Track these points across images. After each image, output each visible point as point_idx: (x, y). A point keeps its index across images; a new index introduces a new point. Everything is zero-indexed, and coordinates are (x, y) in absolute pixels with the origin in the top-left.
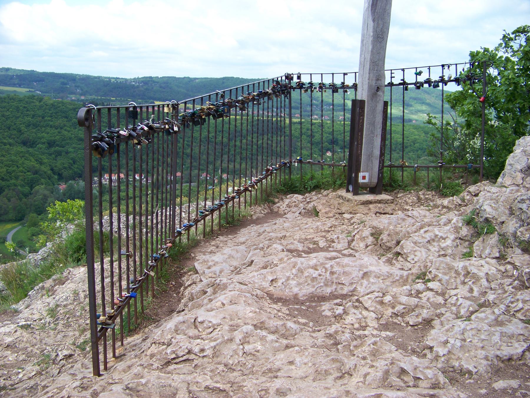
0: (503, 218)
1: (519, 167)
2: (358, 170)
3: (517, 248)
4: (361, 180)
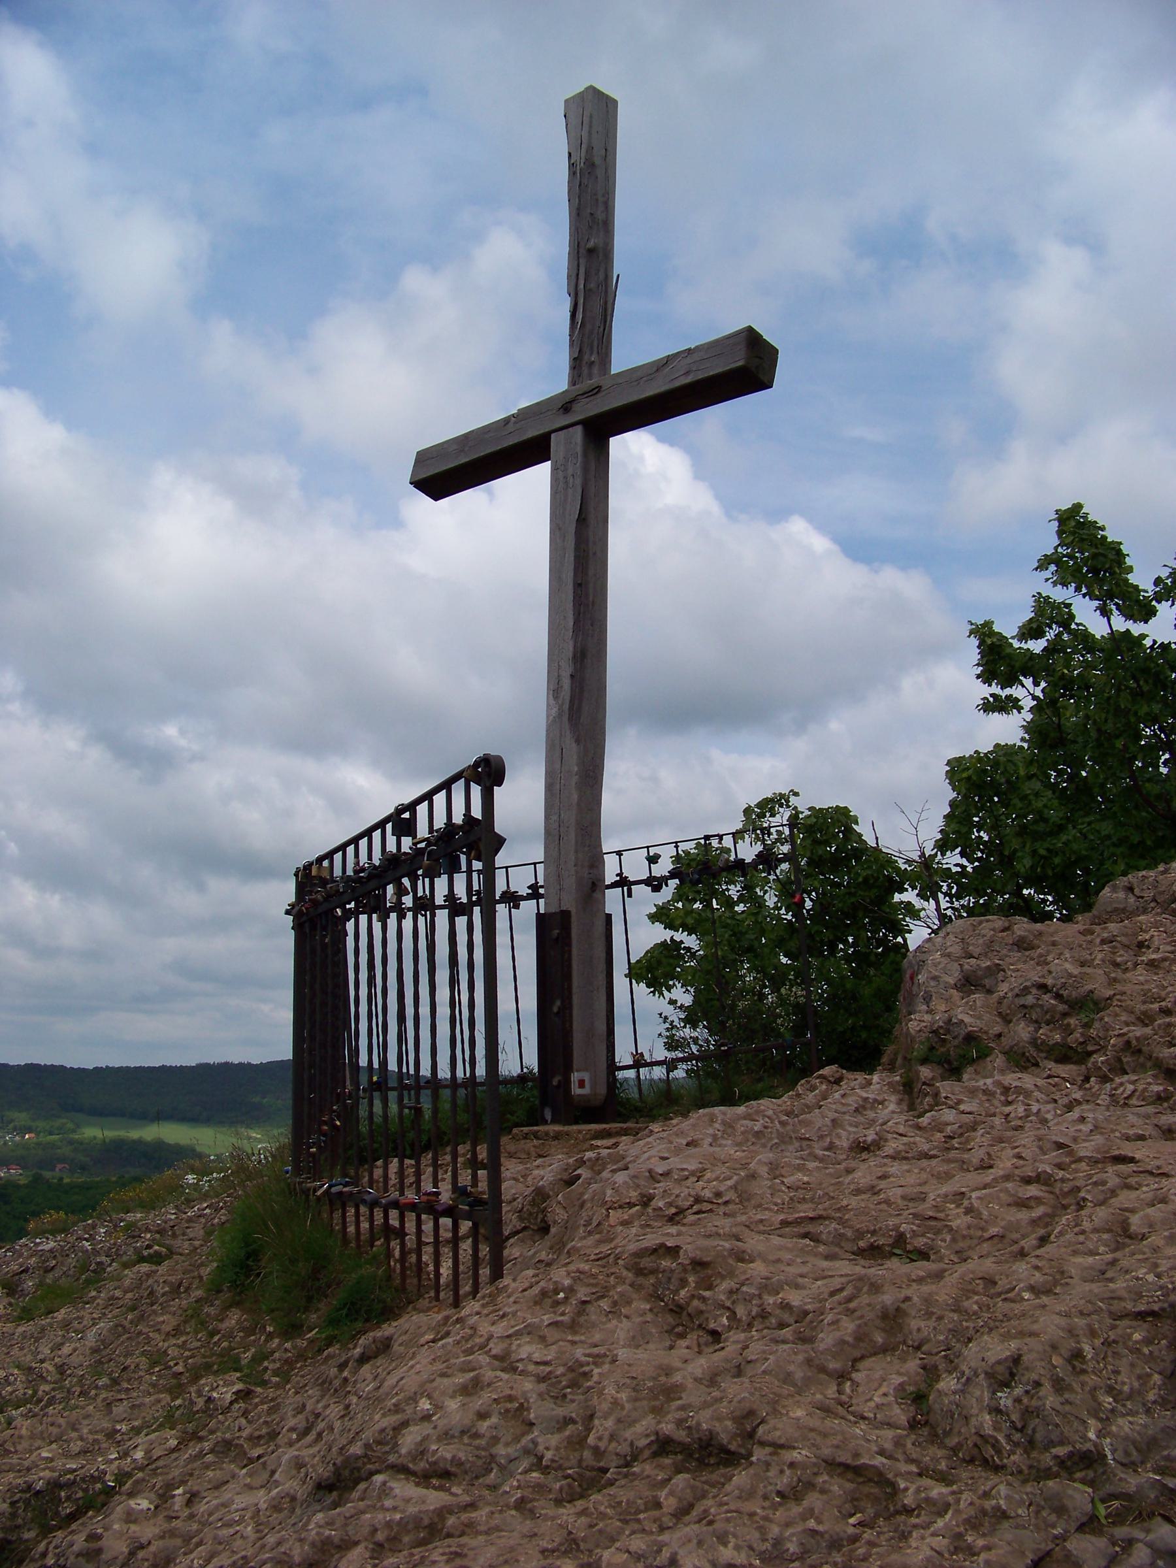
0: (997, 1029)
1: (952, 981)
2: (568, 1068)
3: (1046, 1062)
4: (576, 1090)
